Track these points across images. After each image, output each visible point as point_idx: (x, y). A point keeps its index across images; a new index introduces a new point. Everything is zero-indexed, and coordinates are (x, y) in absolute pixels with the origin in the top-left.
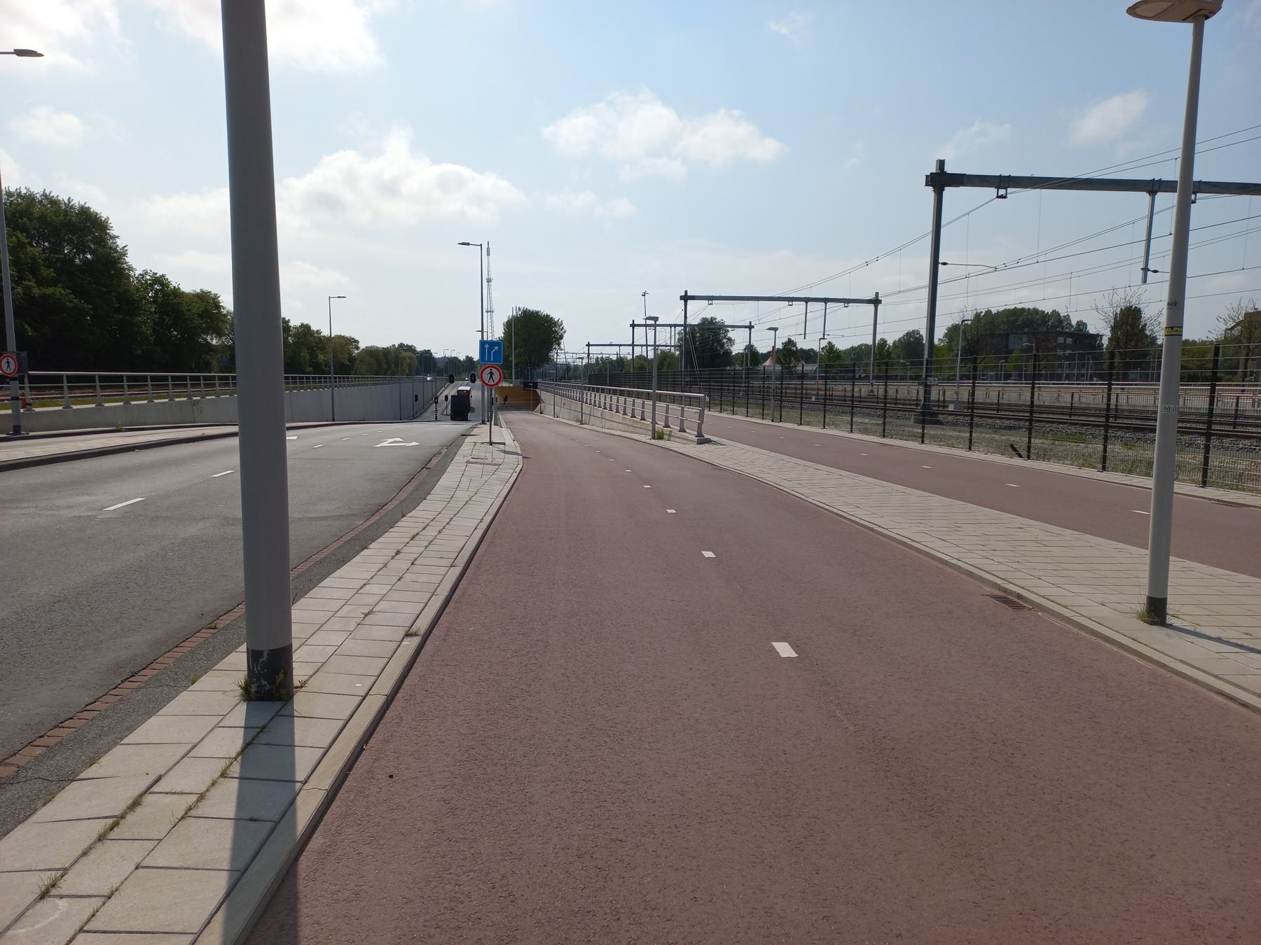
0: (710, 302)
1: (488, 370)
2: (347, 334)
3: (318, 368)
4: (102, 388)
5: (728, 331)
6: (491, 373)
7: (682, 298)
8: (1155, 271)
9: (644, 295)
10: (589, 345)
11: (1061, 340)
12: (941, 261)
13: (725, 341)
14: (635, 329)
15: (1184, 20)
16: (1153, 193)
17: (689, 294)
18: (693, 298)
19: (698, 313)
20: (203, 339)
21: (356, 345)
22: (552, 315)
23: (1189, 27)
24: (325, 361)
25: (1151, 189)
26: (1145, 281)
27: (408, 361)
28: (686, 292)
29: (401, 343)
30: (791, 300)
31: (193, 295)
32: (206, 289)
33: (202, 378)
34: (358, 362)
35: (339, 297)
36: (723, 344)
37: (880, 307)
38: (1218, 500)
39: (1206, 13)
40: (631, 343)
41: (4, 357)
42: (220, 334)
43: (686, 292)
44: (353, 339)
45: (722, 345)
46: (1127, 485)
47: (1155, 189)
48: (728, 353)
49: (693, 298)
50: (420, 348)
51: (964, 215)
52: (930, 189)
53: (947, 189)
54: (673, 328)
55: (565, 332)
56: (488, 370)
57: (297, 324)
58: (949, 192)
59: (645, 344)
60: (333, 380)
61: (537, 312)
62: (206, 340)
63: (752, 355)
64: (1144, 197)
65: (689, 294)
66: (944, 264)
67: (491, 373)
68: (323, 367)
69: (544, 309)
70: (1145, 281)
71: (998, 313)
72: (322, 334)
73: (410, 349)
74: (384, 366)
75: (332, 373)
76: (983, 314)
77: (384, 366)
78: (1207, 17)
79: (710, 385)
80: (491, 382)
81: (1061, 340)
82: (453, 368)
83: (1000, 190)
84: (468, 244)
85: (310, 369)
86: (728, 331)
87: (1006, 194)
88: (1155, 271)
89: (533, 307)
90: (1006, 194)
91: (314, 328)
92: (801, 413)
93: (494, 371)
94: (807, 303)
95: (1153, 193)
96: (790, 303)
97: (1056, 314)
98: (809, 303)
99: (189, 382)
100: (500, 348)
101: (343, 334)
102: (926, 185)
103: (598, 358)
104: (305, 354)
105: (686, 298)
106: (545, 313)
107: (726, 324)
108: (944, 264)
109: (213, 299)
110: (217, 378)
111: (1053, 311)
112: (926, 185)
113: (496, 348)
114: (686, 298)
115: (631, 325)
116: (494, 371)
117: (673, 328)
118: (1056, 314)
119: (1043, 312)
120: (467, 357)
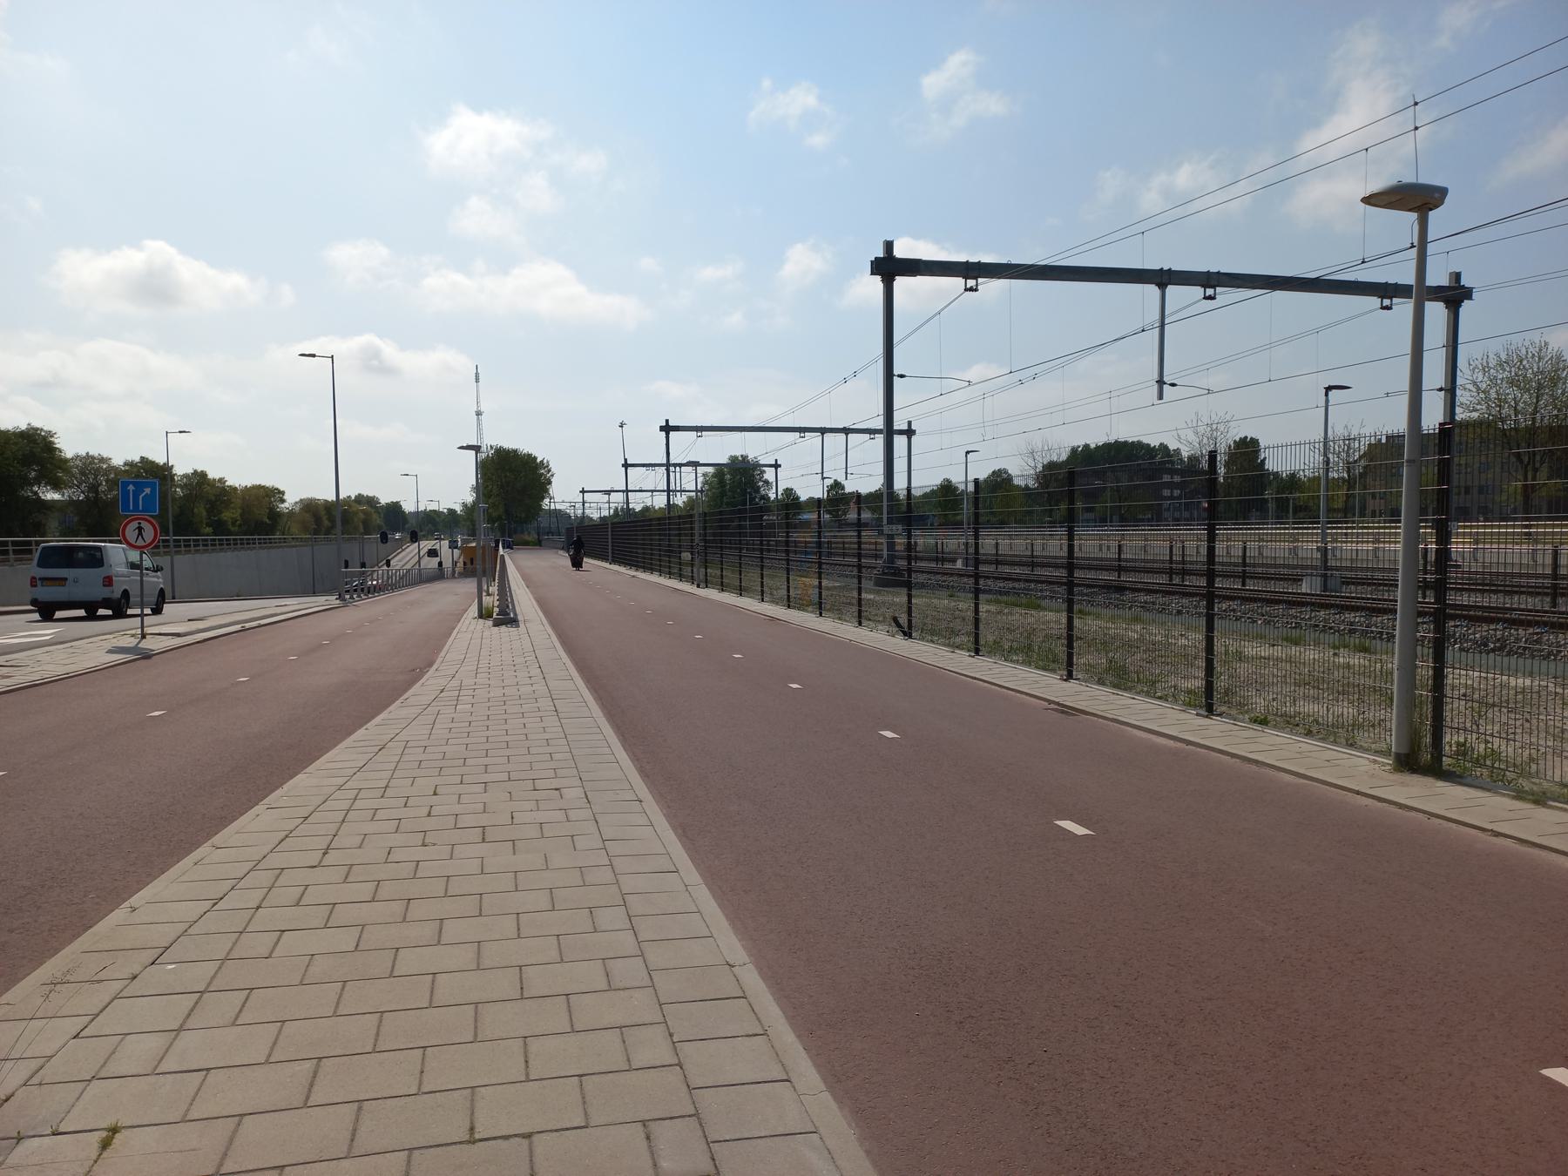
0: (699, 434)
1: (135, 525)
2: (268, 481)
3: (219, 527)
4: (16, 560)
5: (764, 471)
6: (140, 529)
7: (662, 429)
8: (1173, 385)
9: (621, 426)
10: (583, 492)
11: (1167, 478)
12: (896, 372)
13: (761, 484)
14: (628, 471)
15: (1410, 210)
16: (1162, 286)
17: (671, 424)
18: (677, 429)
19: (719, 450)
20: (32, 491)
21: (281, 498)
22: (534, 452)
23: (1414, 216)
24: (232, 518)
25: (1160, 281)
26: (1161, 397)
27: (362, 516)
28: (667, 421)
29: (360, 494)
30: (802, 430)
31: (14, 434)
32: (37, 424)
33: (10, 544)
34: (285, 520)
35: (180, 432)
36: (759, 488)
37: (913, 438)
38: (1058, 704)
39: (1431, 206)
40: (629, 489)
41: (133, 520)
42: (56, 486)
43: (667, 421)
44: (277, 489)
45: (757, 490)
46: (975, 678)
47: (1164, 281)
48: (765, 498)
49: (677, 429)
50: (385, 499)
51: (935, 315)
52: (878, 278)
53: (898, 279)
54: (678, 468)
55: (552, 475)
56: (135, 525)
57: (188, 472)
58: (900, 283)
59: (649, 492)
60: (172, 544)
61: (515, 451)
62: (36, 493)
63: (791, 502)
64: (1152, 290)
65: (671, 424)
66: (902, 376)
67: (140, 529)
68: (230, 527)
69: (524, 445)
70: (1161, 397)
71: (1097, 447)
72: (227, 484)
73: (371, 501)
74: (326, 523)
75: (171, 533)
76: (1080, 449)
77: (326, 523)
78: (1431, 210)
79: (1561, 539)
80: (140, 543)
81: (1167, 478)
82: (431, 524)
83: (1384, 300)
84: (314, 356)
85: (209, 530)
86: (764, 471)
87: (977, 285)
88: (1173, 385)
89: (509, 444)
90: (977, 285)
91: (213, 474)
92: (762, 574)
93: (144, 524)
94: (823, 434)
95: (1162, 286)
96: (872, 436)
97: (1164, 448)
98: (850, 435)
99: (10, 548)
100: (153, 491)
101: (263, 484)
102: (872, 274)
103: (617, 508)
104: (201, 510)
105: (667, 429)
106: (525, 451)
107: (761, 462)
108: (902, 376)
109: (44, 438)
110: (10, 544)
111: (1161, 444)
112: (872, 274)
113: (148, 490)
114: (667, 429)
115: (623, 466)
116: (144, 524)
117: (678, 468)
118: (1164, 447)
119: (1148, 445)
120: (449, 509)
